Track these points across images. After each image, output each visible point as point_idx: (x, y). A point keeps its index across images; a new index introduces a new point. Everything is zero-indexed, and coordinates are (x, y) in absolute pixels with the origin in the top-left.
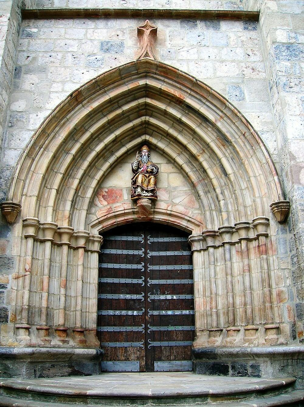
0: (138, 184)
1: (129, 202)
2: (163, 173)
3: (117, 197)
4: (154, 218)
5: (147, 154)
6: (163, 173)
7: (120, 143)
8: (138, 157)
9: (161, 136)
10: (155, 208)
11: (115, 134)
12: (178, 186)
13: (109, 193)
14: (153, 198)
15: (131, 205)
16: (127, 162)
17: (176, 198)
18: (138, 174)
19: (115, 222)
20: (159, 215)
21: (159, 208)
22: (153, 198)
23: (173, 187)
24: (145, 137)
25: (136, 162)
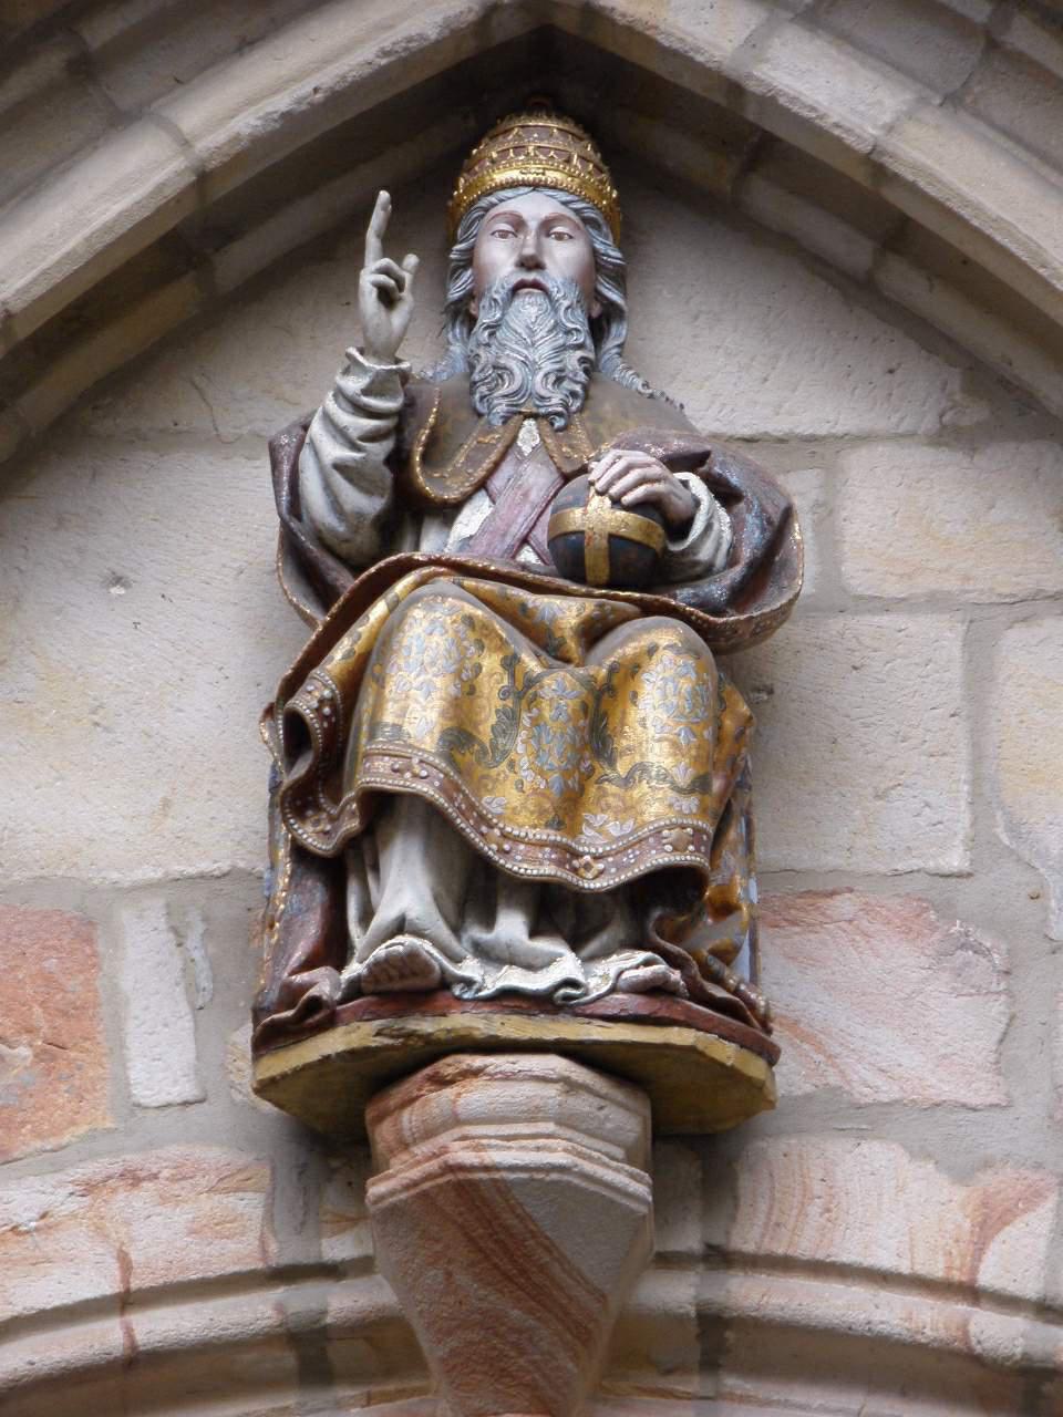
0: (377, 773)
2: (885, 605)
5: (564, 258)
6: (885, 605)
8: (387, 297)
10: (719, 1258)
15: (249, 1206)
18: (379, 609)
21: (805, 1248)
25: (354, 384)
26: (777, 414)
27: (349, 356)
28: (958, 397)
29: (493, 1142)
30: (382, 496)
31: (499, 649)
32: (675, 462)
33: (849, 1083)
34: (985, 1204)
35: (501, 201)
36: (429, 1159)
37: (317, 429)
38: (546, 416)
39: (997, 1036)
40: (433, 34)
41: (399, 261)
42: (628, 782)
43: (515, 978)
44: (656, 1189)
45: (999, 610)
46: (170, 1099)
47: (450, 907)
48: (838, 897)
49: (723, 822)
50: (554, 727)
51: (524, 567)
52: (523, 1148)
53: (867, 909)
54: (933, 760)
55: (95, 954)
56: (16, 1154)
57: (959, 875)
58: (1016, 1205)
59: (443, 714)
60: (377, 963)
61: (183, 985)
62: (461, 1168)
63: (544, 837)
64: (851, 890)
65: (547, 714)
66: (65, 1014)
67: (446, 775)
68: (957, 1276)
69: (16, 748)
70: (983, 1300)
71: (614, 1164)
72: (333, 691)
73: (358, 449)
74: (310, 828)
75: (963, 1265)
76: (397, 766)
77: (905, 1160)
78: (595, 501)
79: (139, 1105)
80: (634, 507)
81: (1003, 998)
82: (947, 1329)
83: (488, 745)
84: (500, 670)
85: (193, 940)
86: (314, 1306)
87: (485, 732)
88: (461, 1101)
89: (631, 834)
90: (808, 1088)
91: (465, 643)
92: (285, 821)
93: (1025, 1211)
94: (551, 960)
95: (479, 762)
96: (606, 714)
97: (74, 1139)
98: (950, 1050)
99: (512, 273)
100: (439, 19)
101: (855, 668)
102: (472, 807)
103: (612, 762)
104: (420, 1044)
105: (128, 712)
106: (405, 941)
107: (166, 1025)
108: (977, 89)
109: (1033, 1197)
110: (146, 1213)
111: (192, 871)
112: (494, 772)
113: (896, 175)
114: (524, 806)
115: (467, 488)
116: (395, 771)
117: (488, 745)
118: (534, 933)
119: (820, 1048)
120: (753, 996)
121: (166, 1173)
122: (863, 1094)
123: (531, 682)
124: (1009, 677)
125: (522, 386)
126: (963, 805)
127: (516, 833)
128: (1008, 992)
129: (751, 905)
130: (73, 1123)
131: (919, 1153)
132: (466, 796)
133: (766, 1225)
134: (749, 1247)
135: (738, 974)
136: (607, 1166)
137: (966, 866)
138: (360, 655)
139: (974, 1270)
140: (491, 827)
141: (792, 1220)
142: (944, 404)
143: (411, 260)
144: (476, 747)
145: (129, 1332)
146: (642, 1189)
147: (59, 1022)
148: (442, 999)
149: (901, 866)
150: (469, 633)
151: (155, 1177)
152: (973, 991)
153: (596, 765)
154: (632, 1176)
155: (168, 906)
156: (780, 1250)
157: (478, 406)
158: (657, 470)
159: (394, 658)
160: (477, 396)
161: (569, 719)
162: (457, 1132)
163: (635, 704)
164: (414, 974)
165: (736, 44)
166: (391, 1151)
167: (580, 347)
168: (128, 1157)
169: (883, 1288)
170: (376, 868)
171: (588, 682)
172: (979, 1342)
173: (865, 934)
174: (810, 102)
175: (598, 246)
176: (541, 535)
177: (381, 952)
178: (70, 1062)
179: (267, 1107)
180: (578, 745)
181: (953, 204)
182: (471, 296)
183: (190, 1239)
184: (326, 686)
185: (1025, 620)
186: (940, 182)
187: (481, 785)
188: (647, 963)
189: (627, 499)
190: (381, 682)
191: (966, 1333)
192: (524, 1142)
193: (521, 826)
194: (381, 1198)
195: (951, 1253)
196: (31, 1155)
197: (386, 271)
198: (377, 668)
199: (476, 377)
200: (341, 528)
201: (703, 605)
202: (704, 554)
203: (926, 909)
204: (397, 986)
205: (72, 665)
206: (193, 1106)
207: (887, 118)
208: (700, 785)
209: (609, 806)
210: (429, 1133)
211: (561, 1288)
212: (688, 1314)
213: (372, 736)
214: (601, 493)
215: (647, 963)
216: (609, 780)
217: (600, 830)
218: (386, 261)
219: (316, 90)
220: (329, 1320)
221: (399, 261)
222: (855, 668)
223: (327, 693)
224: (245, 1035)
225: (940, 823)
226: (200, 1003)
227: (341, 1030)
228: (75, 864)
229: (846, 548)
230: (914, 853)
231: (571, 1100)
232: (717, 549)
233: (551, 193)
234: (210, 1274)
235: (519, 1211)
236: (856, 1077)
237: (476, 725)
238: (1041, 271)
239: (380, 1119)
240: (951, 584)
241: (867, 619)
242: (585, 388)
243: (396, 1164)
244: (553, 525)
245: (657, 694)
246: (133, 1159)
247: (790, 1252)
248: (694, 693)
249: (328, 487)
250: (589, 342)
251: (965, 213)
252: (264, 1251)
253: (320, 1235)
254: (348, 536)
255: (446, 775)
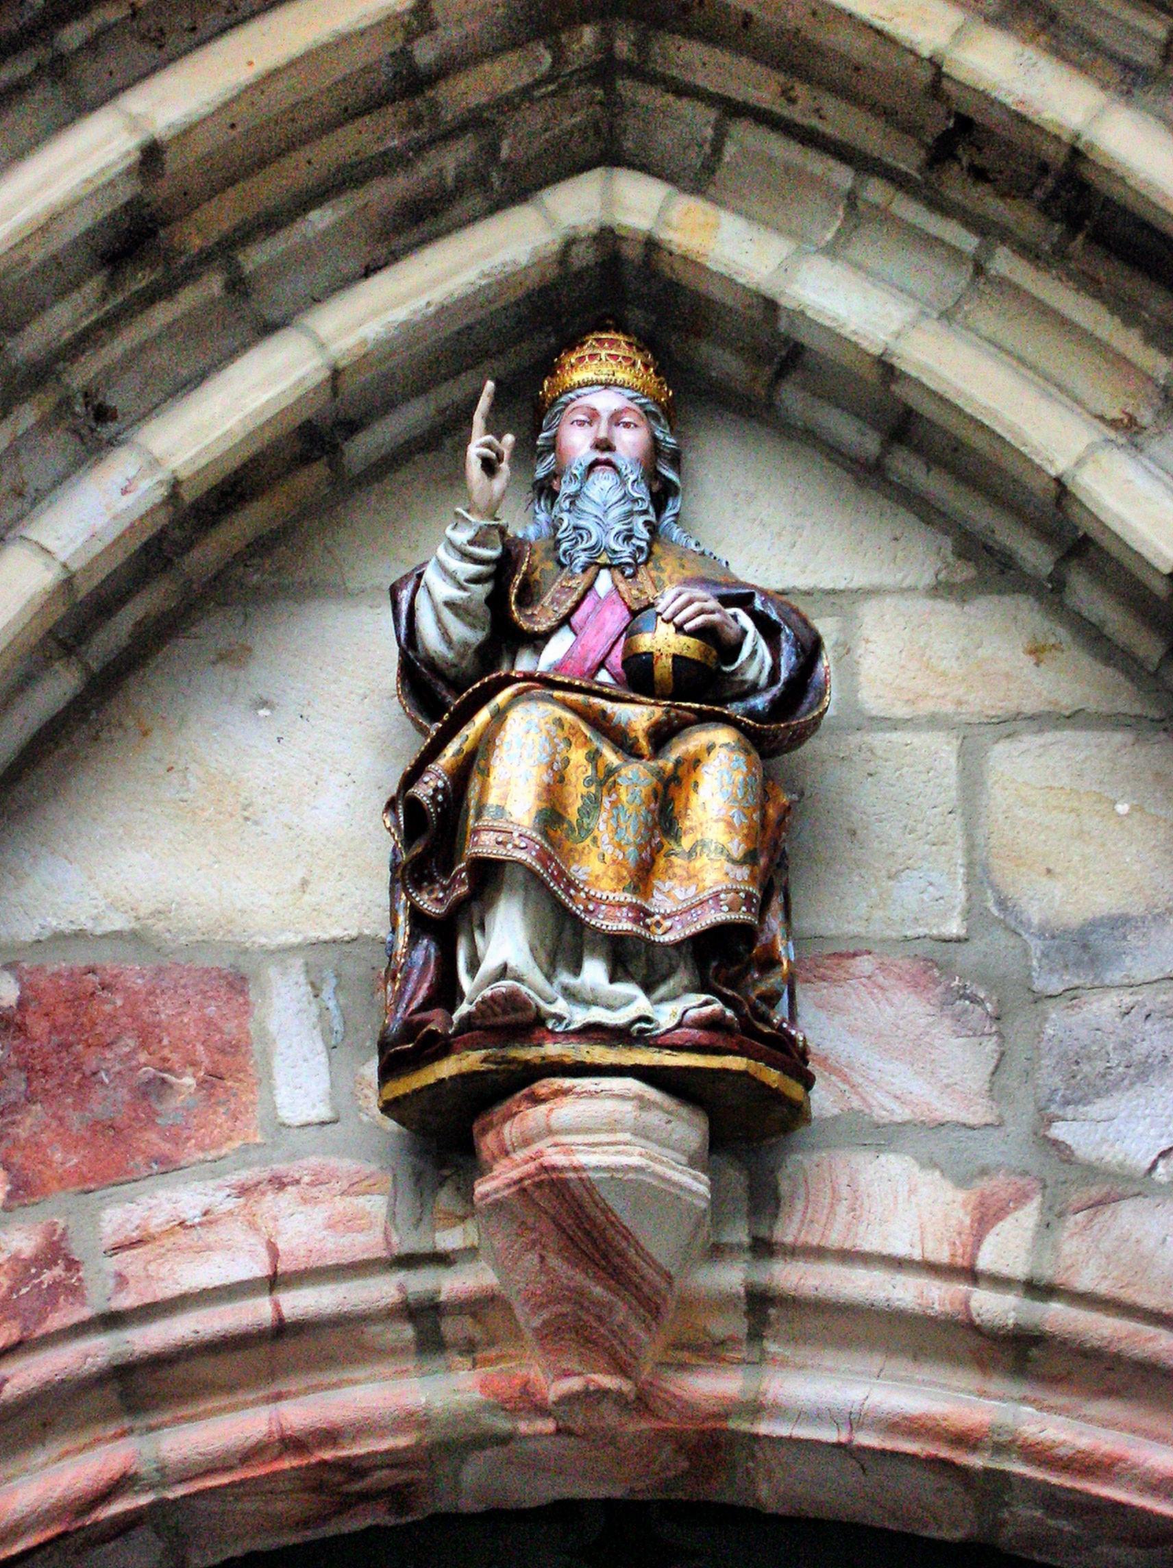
0: (486, 845)
1: (347, 1165)
2: (893, 724)
3: (159, 1087)
4: (756, 1409)
6: (893, 724)
7: (214, 284)
8: (489, 467)
9: (843, 176)
10: (763, 1248)
11: (134, 123)
12: (1137, 910)
13: (39, 1027)
14: (736, 1063)
15: (376, 1205)
16: (341, 592)
17: (1104, 1086)
19: (122, 1484)
20: (829, 1358)
21: (834, 1239)
22: (736, 1063)
23: (1048, 933)
24: (609, 202)
25: (462, 536)
26: (804, 572)
27: (457, 514)
28: (951, 559)
29: (581, 1148)
30: (484, 630)
31: (585, 744)
32: (726, 601)
33: (870, 1107)
34: (982, 1204)
35: (578, 397)
36: (526, 1162)
37: (431, 575)
38: (616, 566)
39: (991, 1068)
40: (523, 260)
41: (499, 438)
42: (691, 854)
43: (598, 1015)
44: (713, 1189)
45: (987, 728)
46: (309, 1119)
47: (543, 956)
48: (858, 958)
49: (768, 892)
50: (631, 810)
51: (600, 684)
52: (604, 1152)
53: (882, 967)
54: (934, 848)
55: (246, 1003)
56: (183, 1163)
57: (958, 940)
58: (1008, 1205)
59: (539, 796)
60: (484, 1001)
61: (318, 1028)
62: (554, 1168)
63: (622, 899)
64: (870, 953)
65: (624, 797)
66: (222, 1051)
67: (542, 847)
68: (960, 1261)
69: (181, 837)
70: (981, 1282)
71: (680, 1167)
72: (445, 783)
73: (465, 589)
74: (426, 897)
75: (964, 1253)
76: (500, 839)
77: (916, 1169)
78: (662, 627)
79: (283, 1125)
80: (692, 633)
81: (995, 1038)
82: (951, 1304)
83: (575, 823)
84: (585, 762)
85: (327, 991)
86: (429, 1287)
87: (573, 814)
88: (554, 1115)
89: (696, 896)
90: (836, 1111)
91: (556, 740)
92: (406, 890)
93: (1015, 1209)
94: (630, 1001)
95: (567, 837)
96: (672, 800)
97: (230, 1152)
98: (951, 1081)
99: (588, 453)
100: (529, 248)
101: (870, 775)
102: (562, 874)
103: (677, 838)
104: (520, 1068)
105: (273, 809)
106: (505, 985)
107: (306, 1060)
108: (966, 308)
109: (1022, 1198)
110: (290, 1211)
111: (326, 937)
112: (580, 846)
113: (902, 373)
114: (605, 873)
115: (552, 622)
116: (498, 843)
117: (575, 823)
118: (613, 979)
119: (845, 1080)
120: (793, 1032)
121: (306, 1179)
122: (881, 1115)
123: (611, 772)
124: (996, 782)
125: (597, 543)
126: (960, 883)
127: (598, 895)
128: (999, 1034)
129: (789, 961)
130: (230, 1139)
131: (930, 1163)
132: (557, 865)
133: (802, 1222)
134: (789, 1239)
135: (779, 1014)
136: (674, 1168)
137: (962, 933)
138: (468, 754)
139: (974, 1256)
140: (578, 890)
141: (824, 1217)
142: (939, 564)
143: (509, 438)
144: (566, 826)
145: (277, 1307)
146: (703, 1189)
147: (217, 1057)
148: (538, 1034)
149: (909, 933)
150: (559, 732)
151: (298, 1182)
152: (971, 1033)
153: (664, 841)
154: (695, 1178)
155: (306, 964)
156: (814, 1240)
157: (562, 559)
158: (713, 604)
159: (497, 752)
160: (561, 550)
161: (643, 803)
162: (549, 1140)
163: (696, 791)
164: (515, 1010)
165: (771, 269)
166: (494, 1158)
167: (645, 512)
168: (275, 1166)
169: (899, 1272)
170: (482, 927)
171: (659, 773)
172: (978, 1315)
173: (881, 988)
174: (831, 314)
175: (658, 434)
176: (616, 658)
177: (487, 992)
178: (226, 1089)
179: (391, 1125)
180: (650, 824)
181: (950, 395)
182: (555, 475)
183: (325, 1233)
184: (439, 777)
185: (1009, 736)
186: (939, 377)
187: (569, 856)
188: (706, 1003)
189: (687, 627)
190: (486, 772)
191: (967, 1307)
192: (606, 1148)
193: (603, 890)
194: (487, 1195)
195: (954, 1244)
196: (194, 1164)
197: (489, 446)
198: (482, 763)
199: (560, 536)
200: (450, 655)
201: (751, 713)
202: (751, 675)
203: (931, 968)
204: (501, 1020)
205: (228, 771)
206: (328, 1127)
207: (894, 327)
208: (750, 858)
209: (675, 875)
210: (526, 1142)
211: (635, 1269)
212: (738, 1292)
213: (479, 816)
214: (667, 621)
215: (706, 1003)
216: (676, 855)
217: (668, 894)
218: (489, 438)
219: (428, 304)
220: (442, 1298)
221: (499, 438)
222: (870, 775)
223: (440, 784)
224: (371, 1069)
225: (941, 898)
226: (333, 1043)
227: (454, 1057)
228: (230, 931)
229: (861, 679)
230: (921, 922)
231: (644, 1114)
232: (761, 672)
233: (619, 390)
234: (343, 1261)
235: (602, 1205)
236: (875, 1103)
237: (565, 808)
238: (1022, 449)
239: (484, 1131)
240: (949, 708)
241: (880, 735)
242: (650, 544)
243: (498, 1168)
244: (628, 647)
245: (716, 784)
246: (280, 1167)
247: (822, 1244)
248: (746, 784)
249: (439, 620)
250: (651, 510)
251: (959, 402)
252: (389, 1243)
253: (434, 1230)
254: (455, 661)
255: (542, 847)
